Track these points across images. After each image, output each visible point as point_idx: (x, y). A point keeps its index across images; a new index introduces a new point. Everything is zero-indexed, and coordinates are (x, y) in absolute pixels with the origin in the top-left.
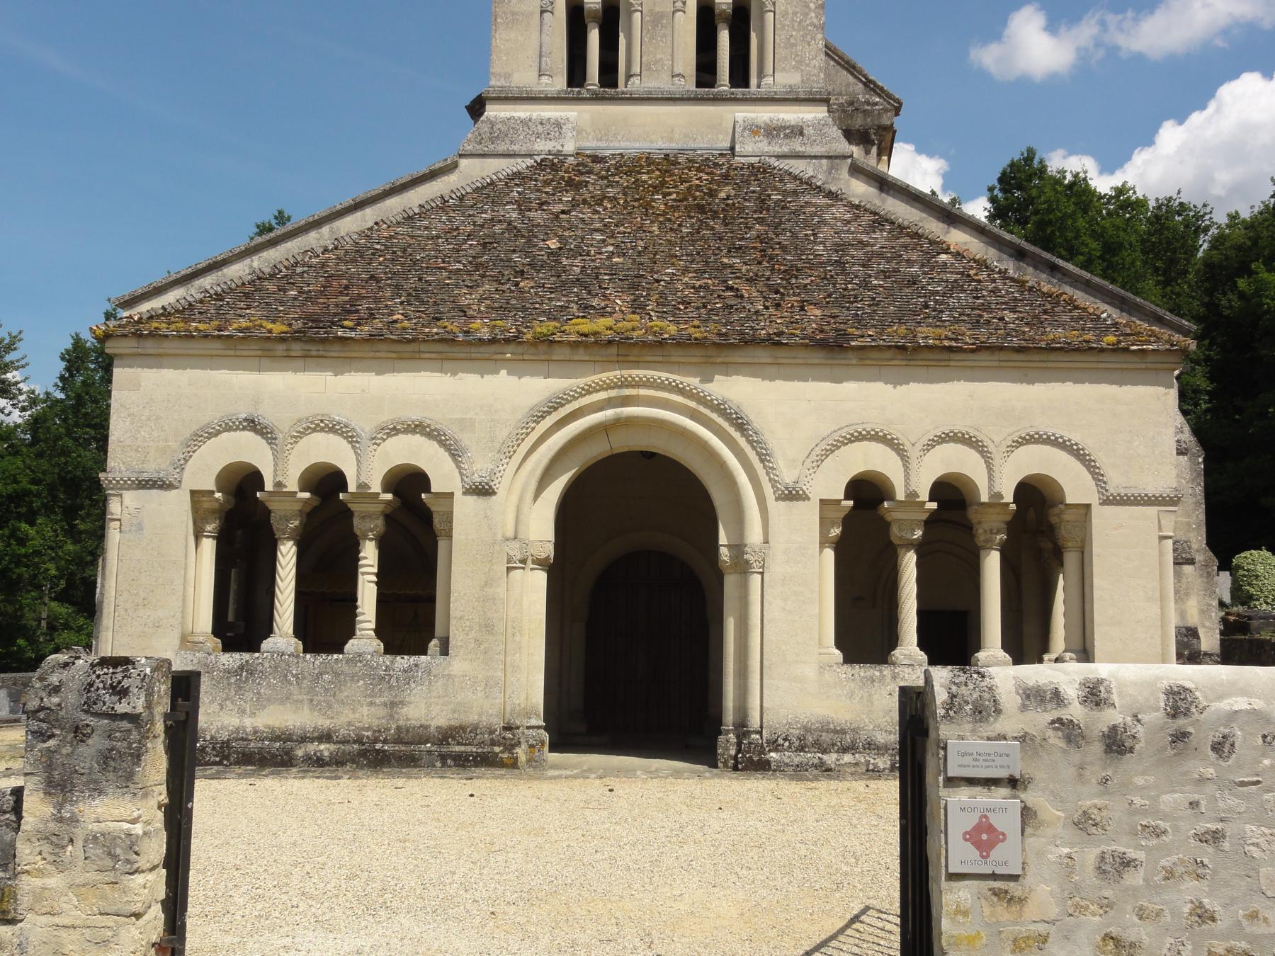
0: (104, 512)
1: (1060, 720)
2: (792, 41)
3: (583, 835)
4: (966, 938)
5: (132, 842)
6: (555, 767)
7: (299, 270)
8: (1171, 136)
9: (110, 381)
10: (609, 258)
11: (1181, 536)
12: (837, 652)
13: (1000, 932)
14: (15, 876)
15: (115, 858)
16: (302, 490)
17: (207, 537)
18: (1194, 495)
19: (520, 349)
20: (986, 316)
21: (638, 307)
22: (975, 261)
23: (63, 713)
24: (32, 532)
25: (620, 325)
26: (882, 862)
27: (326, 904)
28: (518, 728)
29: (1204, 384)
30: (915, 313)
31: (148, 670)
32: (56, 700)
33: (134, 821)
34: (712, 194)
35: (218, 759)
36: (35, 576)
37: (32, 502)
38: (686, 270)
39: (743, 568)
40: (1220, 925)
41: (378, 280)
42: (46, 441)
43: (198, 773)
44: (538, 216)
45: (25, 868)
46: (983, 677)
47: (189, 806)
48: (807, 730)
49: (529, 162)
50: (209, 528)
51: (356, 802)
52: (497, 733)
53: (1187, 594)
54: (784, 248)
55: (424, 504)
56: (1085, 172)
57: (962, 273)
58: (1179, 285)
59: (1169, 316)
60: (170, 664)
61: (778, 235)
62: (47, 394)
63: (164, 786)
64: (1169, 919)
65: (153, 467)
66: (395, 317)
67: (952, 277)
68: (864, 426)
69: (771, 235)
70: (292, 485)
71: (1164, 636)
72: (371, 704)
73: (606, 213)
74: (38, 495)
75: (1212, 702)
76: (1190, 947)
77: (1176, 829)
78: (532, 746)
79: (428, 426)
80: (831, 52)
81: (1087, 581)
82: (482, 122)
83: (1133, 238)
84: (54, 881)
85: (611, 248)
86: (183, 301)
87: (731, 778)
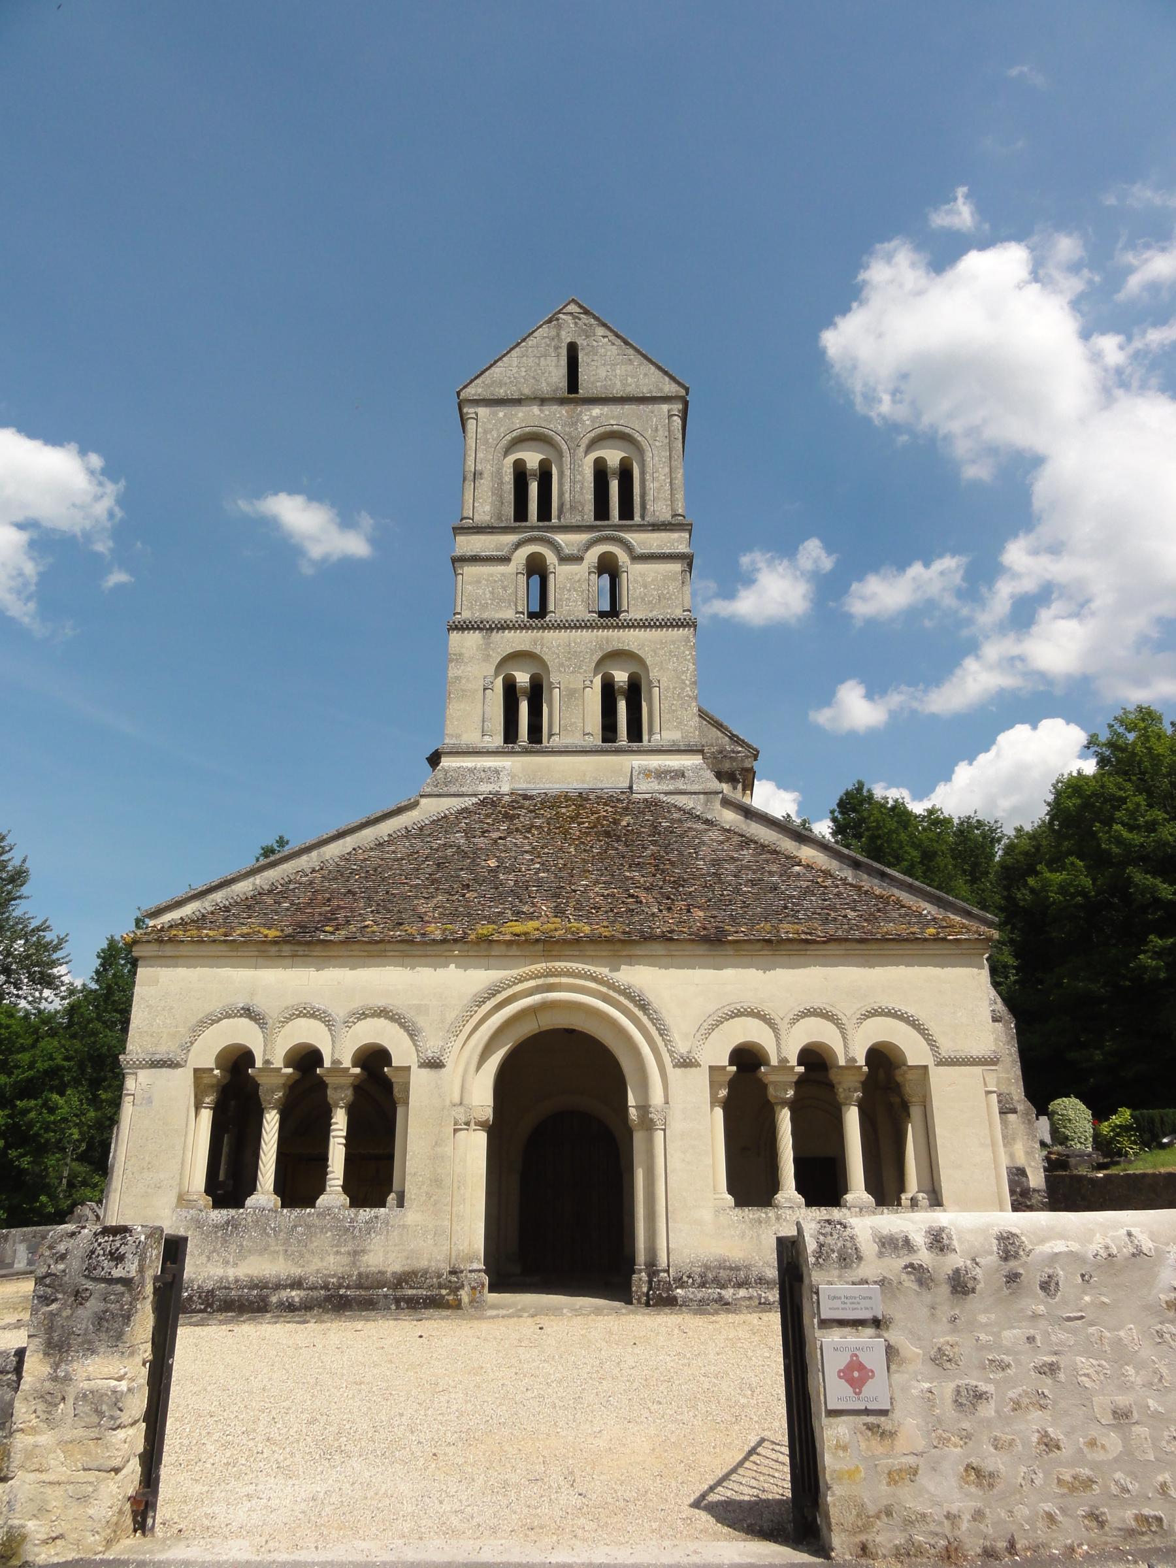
0: (121, 1087)
1: (911, 1265)
2: (673, 708)
3: (516, 1374)
4: (847, 1472)
5: (116, 1398)
6: (493, 1307)
7: (292, 886)
8: (963, 773)
9: (135, 974)
10: (536, 873)
11: (1004, 1089)
12: (729, 1197)
13: (876, 1465)
14: (11, 1434)
15: (100, 1414)
16: (286, 1066)
17: (206, 1108)
18: (1010, 1055)
19: (466, 947)
20: (833, 914)
21: (559, 912)
22: (822, 871)
23: (66, 1279)
24: (61, 1101)
25: (545, 926)
26: (774, 1393)
27: (288, 1450)
28: (462, 1272)
29: (1011, 961)
30: (777, 913)
31: (143, 1238)
32: (61, 1267)
33: (120, 1379)
34: (616, 822)
35: (202, 1307)
36: (60, 1140)
37: (63, 1076)
38: (596, 883)
39: (648, 1125)
40: (1067, 1452)
41: (354, 894)
42: (79, 1023)
43: (180, 1322)
44: (481, 842)
45: (21, 1426)
46: (845, 1227)
47: (170, 1362)
48: (707, 1267)
49: (474, 800)
50: (207, 1100)
51: (320, 1346)
52: (444, 1277)
53: (1014, 1139)
54: (672, 864)
55: (387, 1076)
56: (903, 798)
57: (812, 881)
58: (982, 882)
59: (975, 911)
60: (162, 1231)
61: (667, 854)
62: (84, 985)
63: (150, 1344)
64: (1020, 1448)
65: (164, 1050)
66: (366, 923)
67: (805, 884)
68: (742, 1004)
69: (663, 853)
70: (278, 1062)
71: (998, 1177)
72: (337, 1253)
73: (534, 838)
74: (69, 1070)
75: (1036, 1245)
76: (1041, 1475)
77: (1018, 1362)
78: (473, 1288)
79: (391, 1011)
80: (703, 714)
81: (930, 1133)
82: (439, 770)
83: (944, 847)
84: (45, 1439)
85: (537, 866)
86: (197, 913)
87: (644, 1314)
